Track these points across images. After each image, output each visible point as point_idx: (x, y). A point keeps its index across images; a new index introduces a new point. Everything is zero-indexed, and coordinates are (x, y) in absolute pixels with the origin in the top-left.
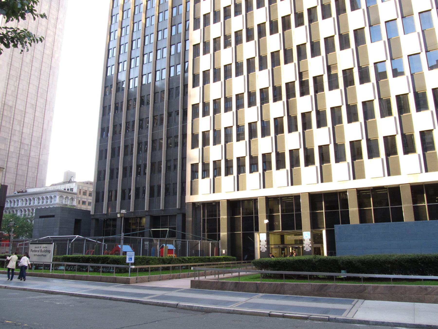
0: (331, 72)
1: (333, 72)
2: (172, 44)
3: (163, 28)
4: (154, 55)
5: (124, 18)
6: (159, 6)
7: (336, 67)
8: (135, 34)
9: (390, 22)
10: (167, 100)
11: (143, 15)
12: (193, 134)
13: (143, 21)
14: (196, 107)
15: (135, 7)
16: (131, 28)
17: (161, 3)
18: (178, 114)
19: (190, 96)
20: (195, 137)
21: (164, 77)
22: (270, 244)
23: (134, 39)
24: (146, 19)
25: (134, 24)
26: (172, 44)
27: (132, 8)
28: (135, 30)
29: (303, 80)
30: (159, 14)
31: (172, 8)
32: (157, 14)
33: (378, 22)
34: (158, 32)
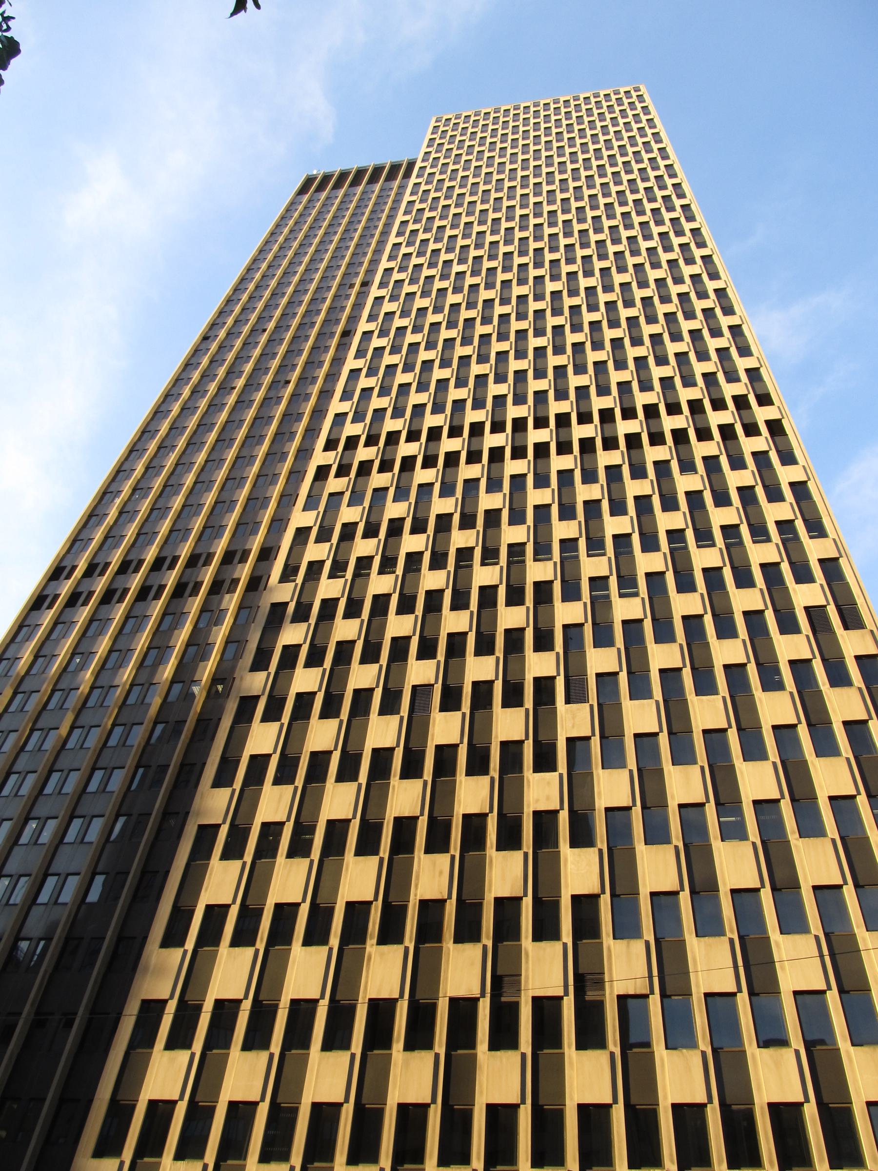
0: (585, 994)
1: (591, 995)
2: (77, 813)
3: (112, 765)
4: (106, 825)
5: (12, 709)
6: (120, 708)
7: (600, 984)
8: (24, 757)
9: (743, 894)
10: (50, 971)
11: (69, 718)
12: (114, 1100)
13: (64, 730)
14: (152, 1010)
15: (53, 691)
16: (19, 739)
17: (128, 702)
18: (69, 1024)
19: (146, 969)
20: (119, 1112)
21: (67, 896)
22: (751, 963)
23: (16, 768)
24: (73, 728)
25: (32, 730)
26: (77, 813)
27: (46, 690)
28: (29, 747)
29: (503, 999)
30: (114, 725)
31: (156, 723)
32: (109, 726)
33: (714, 888)
34: (94, 769)
